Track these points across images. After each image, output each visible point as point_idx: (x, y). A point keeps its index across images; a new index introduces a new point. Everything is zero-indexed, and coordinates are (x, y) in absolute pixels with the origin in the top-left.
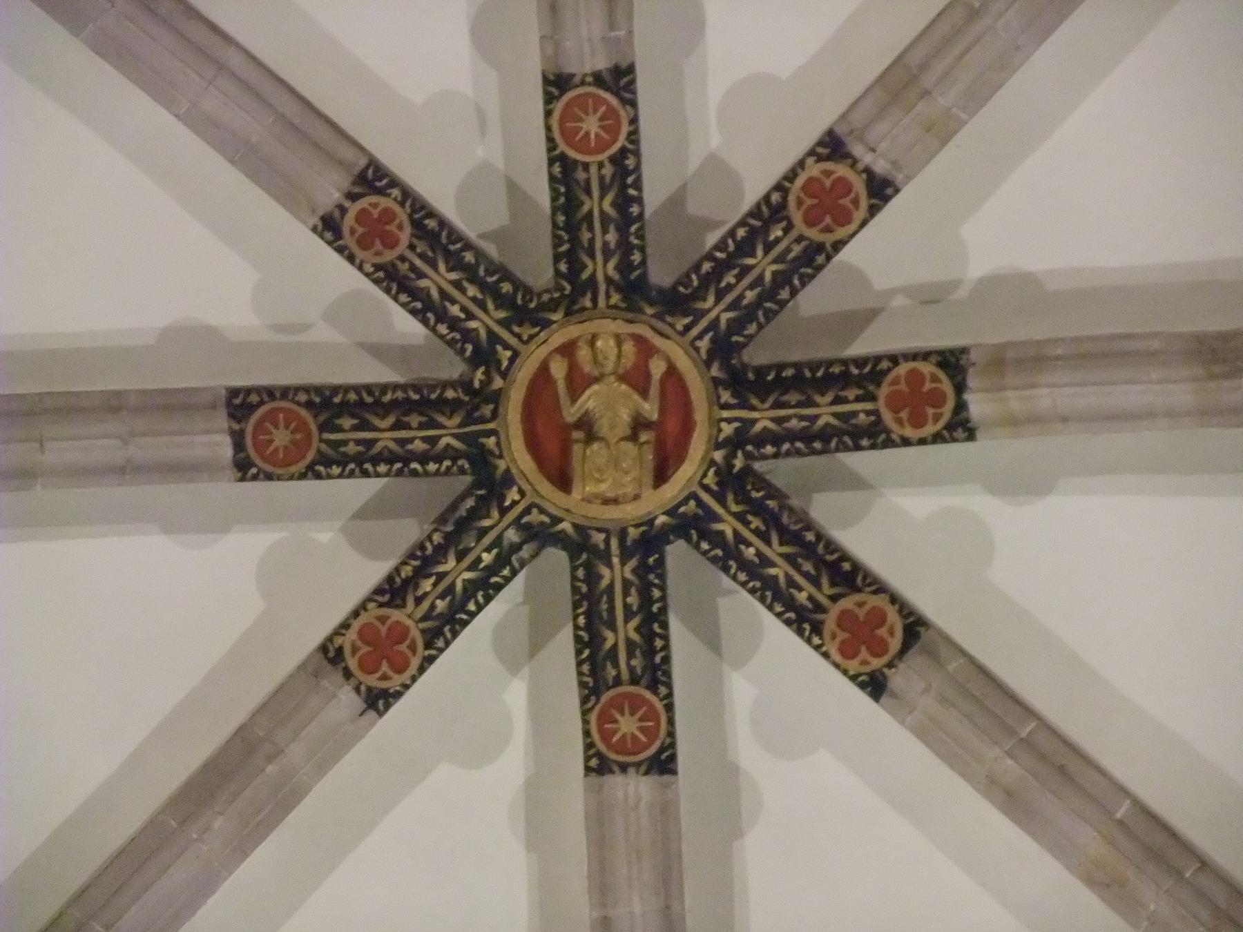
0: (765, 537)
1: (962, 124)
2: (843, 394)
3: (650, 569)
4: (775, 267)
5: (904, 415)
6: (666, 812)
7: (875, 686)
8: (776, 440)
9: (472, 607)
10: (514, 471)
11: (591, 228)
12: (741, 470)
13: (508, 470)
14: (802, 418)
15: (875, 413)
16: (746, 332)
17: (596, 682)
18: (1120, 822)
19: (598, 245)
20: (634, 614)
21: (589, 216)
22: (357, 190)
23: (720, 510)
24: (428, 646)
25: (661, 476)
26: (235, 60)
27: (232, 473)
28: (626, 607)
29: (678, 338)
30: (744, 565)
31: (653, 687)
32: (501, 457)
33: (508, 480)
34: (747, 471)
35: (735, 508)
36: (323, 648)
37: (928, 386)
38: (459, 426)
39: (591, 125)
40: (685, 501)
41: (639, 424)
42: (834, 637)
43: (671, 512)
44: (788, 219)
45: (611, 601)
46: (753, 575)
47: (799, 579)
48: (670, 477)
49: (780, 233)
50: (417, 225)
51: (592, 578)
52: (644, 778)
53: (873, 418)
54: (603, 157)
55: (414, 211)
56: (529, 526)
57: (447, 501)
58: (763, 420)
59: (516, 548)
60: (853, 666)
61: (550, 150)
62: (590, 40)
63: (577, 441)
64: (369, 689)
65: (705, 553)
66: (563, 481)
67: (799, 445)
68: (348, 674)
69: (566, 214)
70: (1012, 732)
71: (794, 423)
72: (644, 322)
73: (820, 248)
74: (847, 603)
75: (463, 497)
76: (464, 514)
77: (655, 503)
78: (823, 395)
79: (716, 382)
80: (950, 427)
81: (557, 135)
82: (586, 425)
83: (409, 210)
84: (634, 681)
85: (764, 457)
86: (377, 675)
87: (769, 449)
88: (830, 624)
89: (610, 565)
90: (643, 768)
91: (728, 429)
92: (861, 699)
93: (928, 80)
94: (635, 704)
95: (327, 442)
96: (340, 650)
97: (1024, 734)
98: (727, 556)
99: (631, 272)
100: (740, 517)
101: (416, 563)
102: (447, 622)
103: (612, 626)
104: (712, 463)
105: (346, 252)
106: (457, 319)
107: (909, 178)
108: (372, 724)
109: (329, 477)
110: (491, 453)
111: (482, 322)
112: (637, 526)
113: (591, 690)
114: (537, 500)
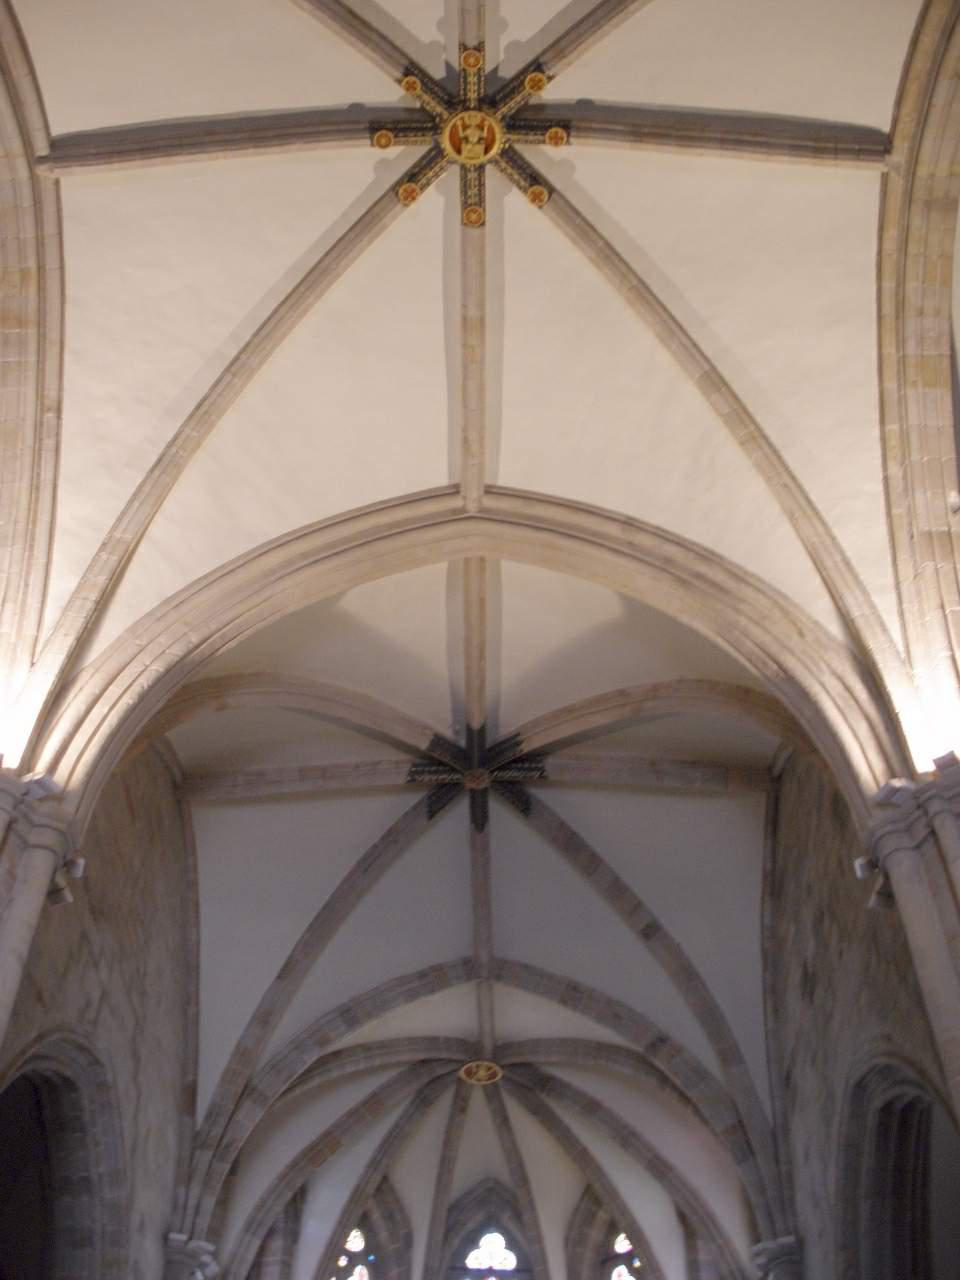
25: (487, 151)
39: (472, 61)
41: (480, 139)
50: (422, 81)
58: (483, 79)
66: (459, 151)
74: (535, 187)
77: (483, 159)
92: (552, 82)
94: (475, 212)
113: (465, 205)
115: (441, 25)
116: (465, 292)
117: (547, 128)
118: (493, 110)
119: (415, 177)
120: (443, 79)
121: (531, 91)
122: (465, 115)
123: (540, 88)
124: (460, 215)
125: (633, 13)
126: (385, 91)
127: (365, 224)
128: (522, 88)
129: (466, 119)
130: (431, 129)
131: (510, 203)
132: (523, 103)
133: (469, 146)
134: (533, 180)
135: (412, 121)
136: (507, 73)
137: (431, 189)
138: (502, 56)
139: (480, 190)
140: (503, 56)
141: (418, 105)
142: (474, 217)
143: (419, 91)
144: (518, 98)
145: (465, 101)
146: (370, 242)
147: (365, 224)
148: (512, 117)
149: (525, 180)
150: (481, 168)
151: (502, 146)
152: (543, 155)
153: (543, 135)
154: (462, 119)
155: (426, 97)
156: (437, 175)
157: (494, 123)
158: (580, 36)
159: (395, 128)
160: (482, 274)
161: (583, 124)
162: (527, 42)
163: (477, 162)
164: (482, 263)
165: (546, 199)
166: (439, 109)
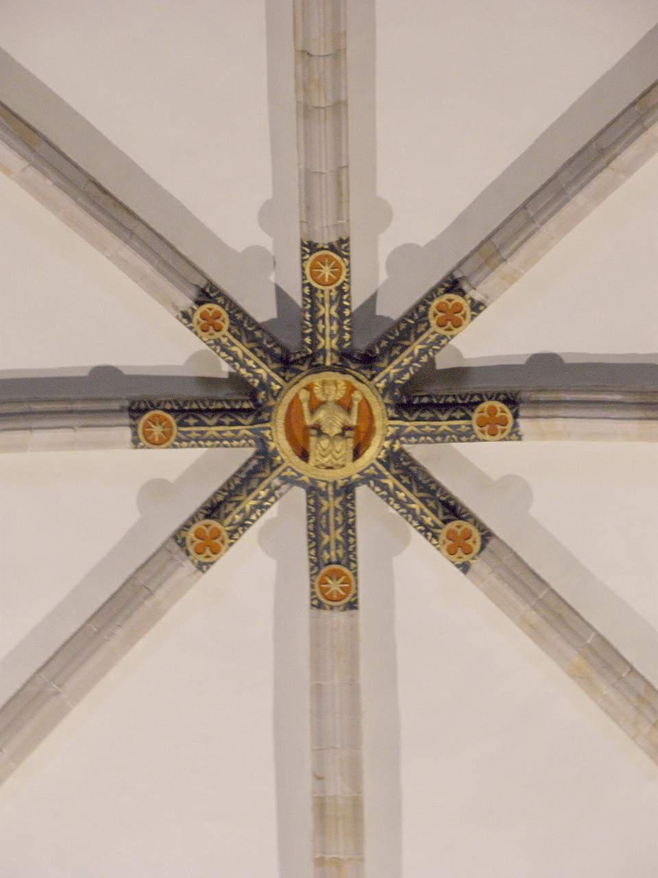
0: (409, 488)
1: (521, 274)
2: (454, 415)
3: (348, 501)
4: (420, 347)
5: (486, 428)
6: (354, 629)
7: (465, 567)
8: (417, 436)
9: (253, 517)
10: (278, 449)
11: (324, 323)
12: (398, 450)
13: (275, 449)
14: (432, 426)
15: (471, 426)
16: (403, 378)
17: (318, 559)
18: (589, 646)
19: (327, 333)
20: (340, 526)
21: (323, 317)
22: (201, 299)
23: (387, 473)
24: (231, 537)
25: (357, 454)
26: (140, 229)
27: (130, 444)
28: (336, 522)
29: (368, 383)
30: (398, 501)
31: (348, 566)
32: (272, 441)
33: (275, 453)
34: (401, 450)
35: (395, 472)
36: (175, 537)
37: (499, 414)
38: (251, 424)
39: (326, 271)
40: (368, 468)
41: (346, 428)
42: (444, 543)
43: (361, 473)
44: (428, 321)
45: (328, 519)
46: (403, 506)
47: (426, 510)
48: (363, 454)
49: (423, 329)
50: (232, 317)
51: (317, 505)
52: (341, 613)
53: (468, 428)
54: (332, 287)
55: (230, 309)
56: (285, 477)
57: (243, 461)
59: (278, 488)
60: (454, 558)
61: (303, 280)
62: (327, 227)
63: (312, 435)
64: (199, 562)
65: (377, 493)
66: (304, 456)
67: (429, 438)
68: (188, 554)
69: (311, 313)
70: (534, 595)
71: (427, 429)
72: (350, 374)
73: (444, 337)
74: (452, 525)
75: (250, 460)
76: (252, 468)
77: (353, 470)
78: (443, 414)
79: (387, 405)
80: (510, 434)
81: (307, 271)
82: (318, 428)
83: (227, 309)
84: (338, 563)
85: (409, 443)
86: (204, 555)
87: (413, 439)
88: (443, 537)
89: (327, 499)
90: (342, 608)
91: (392, 431)
93: (504, 254)
95: (179, 431)
96: (184, 539)
97: (541, 596)
98: (389, 495)
99: (343, 344)
100: (397, 477)
101: (226, 494)
102: (233, 491)
103: (328, 532)
104: (384, 448)
105: (194, 330)
106: (251, 367)
107: (492, 301)
108: (199, 577)
109: (181, 447)
110: (267, 438)
111: (265, 371)
112: (342, 480)
113: (316, 564)
114: (290, 465)
115: (267, 216)
116: (320, 747)
117: (472, 405)
118: (368, 373)
119: (221, 512)
120: (271, 322)
121: (441, 331)
122: (316, 379)
123: (458, 325)
124: (307, 584)
125: (629, 171)
126: (170, 348)
127: (123, 606)
128: (422, 327)
129: (317, 389)
130: (248, 412)
131: (403, 562)
132: (424, 359)
133: (325, 443)
134: (444, 513)
135: (212, 401)
136: (393, 308)
137: (249, 537)
138: (383, 276)
139: (346, 536)
140: (383, 279)
141: (225, 369)
142: (334, 586)
143: (225, 336)
144: (416, 348)
145: (312, 357)
146: (131, 641)
147: (123, 606)
148: (407, 388)
149: (435, 512)
150: (348, 490)
151: (387, 444)
152: (469, 463)
153: (468, 418)
154: (309, 388)
155: (239, 349)
156: (261, 507)
157: (369, 392)
158: (531, 220)
159: (182, 411)
160: (354, 710)
161: (542, 396)
162: (425, 246)
163: (339, 475)
164: (353, 687)
165: (476, 548)
166: (264, 371)
